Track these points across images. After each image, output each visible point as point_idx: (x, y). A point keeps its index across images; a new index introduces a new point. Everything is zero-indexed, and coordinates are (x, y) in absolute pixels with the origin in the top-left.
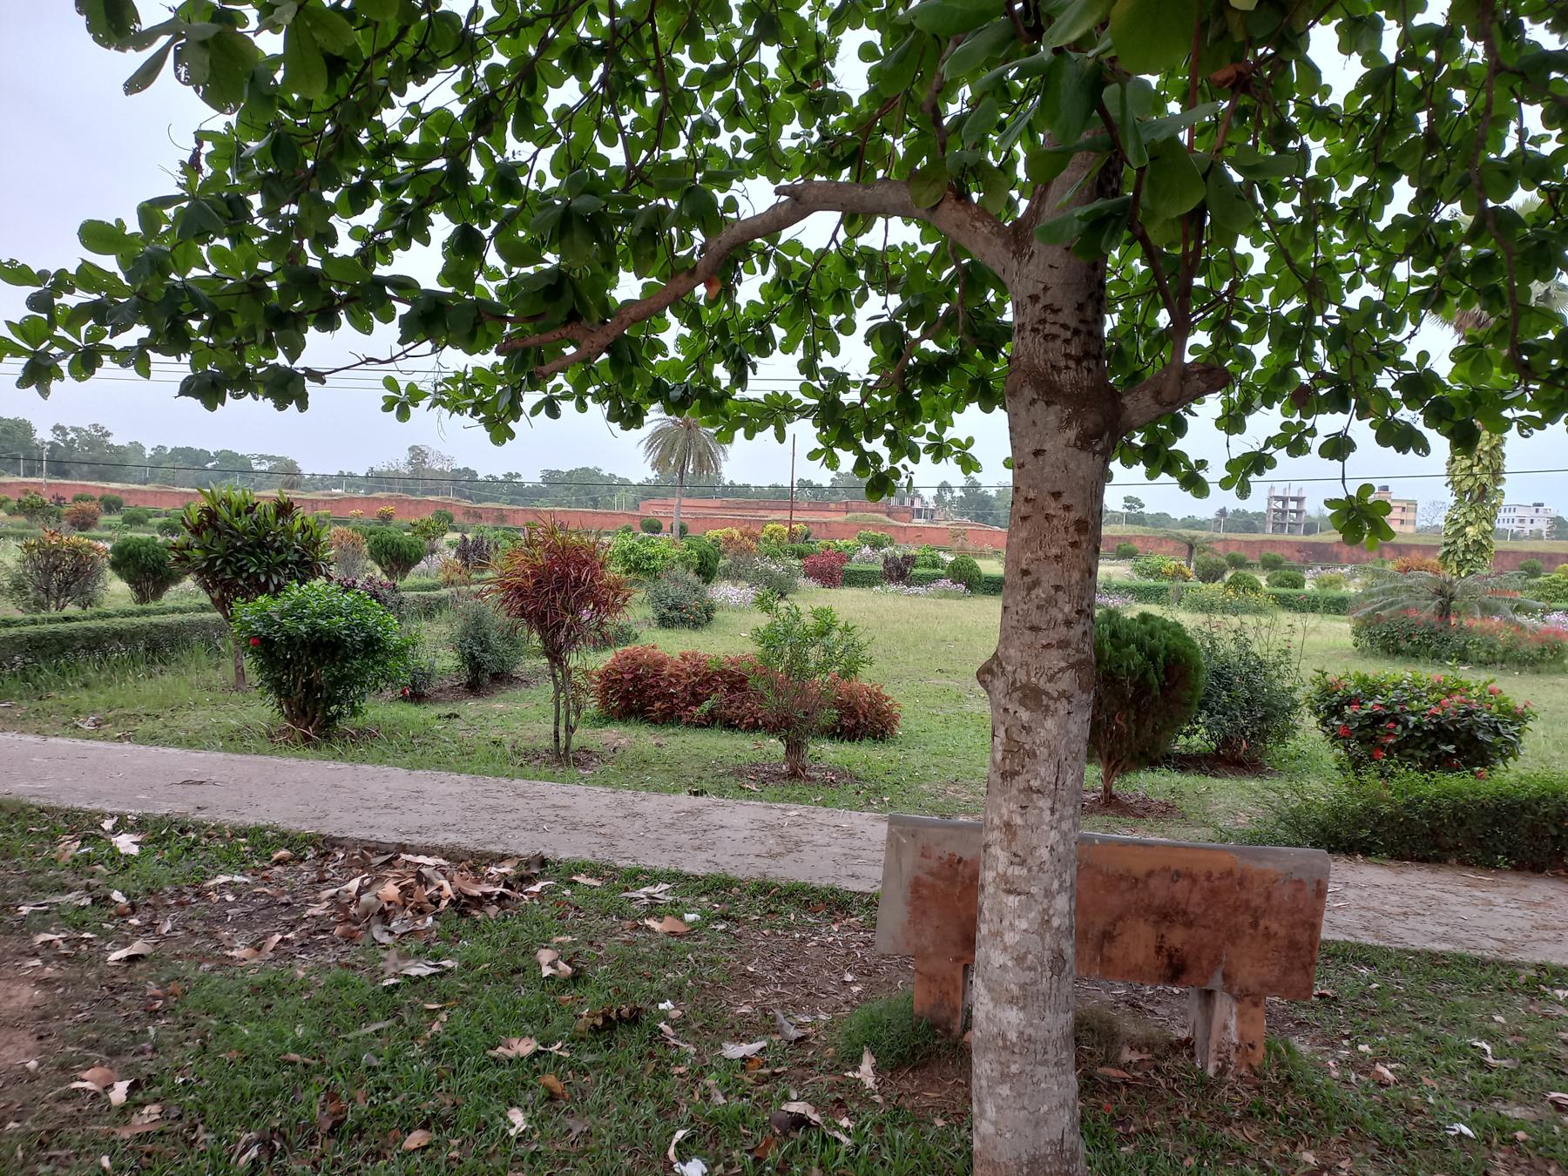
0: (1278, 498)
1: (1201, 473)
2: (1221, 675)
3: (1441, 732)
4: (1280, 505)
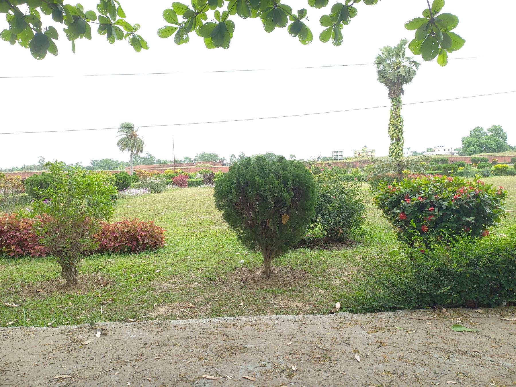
0: (335, 152)
1: (303, 20)
2: (325, 196)
3: (463, 210)
4: (335, 154)
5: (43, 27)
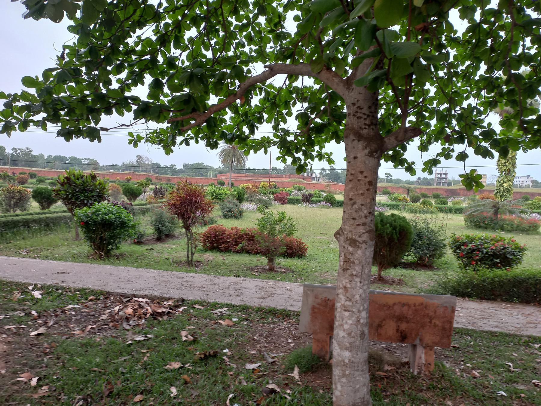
0: (438, 174)
4: (439, 176)
5: (154, 27)
